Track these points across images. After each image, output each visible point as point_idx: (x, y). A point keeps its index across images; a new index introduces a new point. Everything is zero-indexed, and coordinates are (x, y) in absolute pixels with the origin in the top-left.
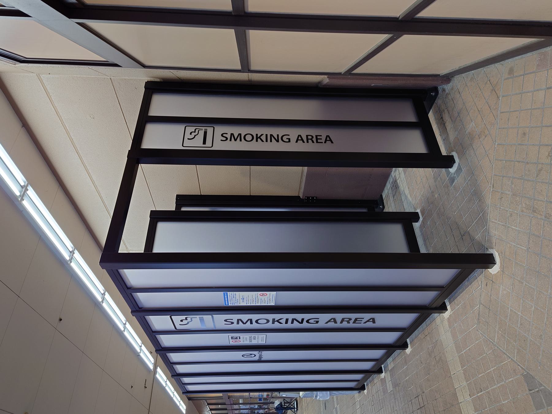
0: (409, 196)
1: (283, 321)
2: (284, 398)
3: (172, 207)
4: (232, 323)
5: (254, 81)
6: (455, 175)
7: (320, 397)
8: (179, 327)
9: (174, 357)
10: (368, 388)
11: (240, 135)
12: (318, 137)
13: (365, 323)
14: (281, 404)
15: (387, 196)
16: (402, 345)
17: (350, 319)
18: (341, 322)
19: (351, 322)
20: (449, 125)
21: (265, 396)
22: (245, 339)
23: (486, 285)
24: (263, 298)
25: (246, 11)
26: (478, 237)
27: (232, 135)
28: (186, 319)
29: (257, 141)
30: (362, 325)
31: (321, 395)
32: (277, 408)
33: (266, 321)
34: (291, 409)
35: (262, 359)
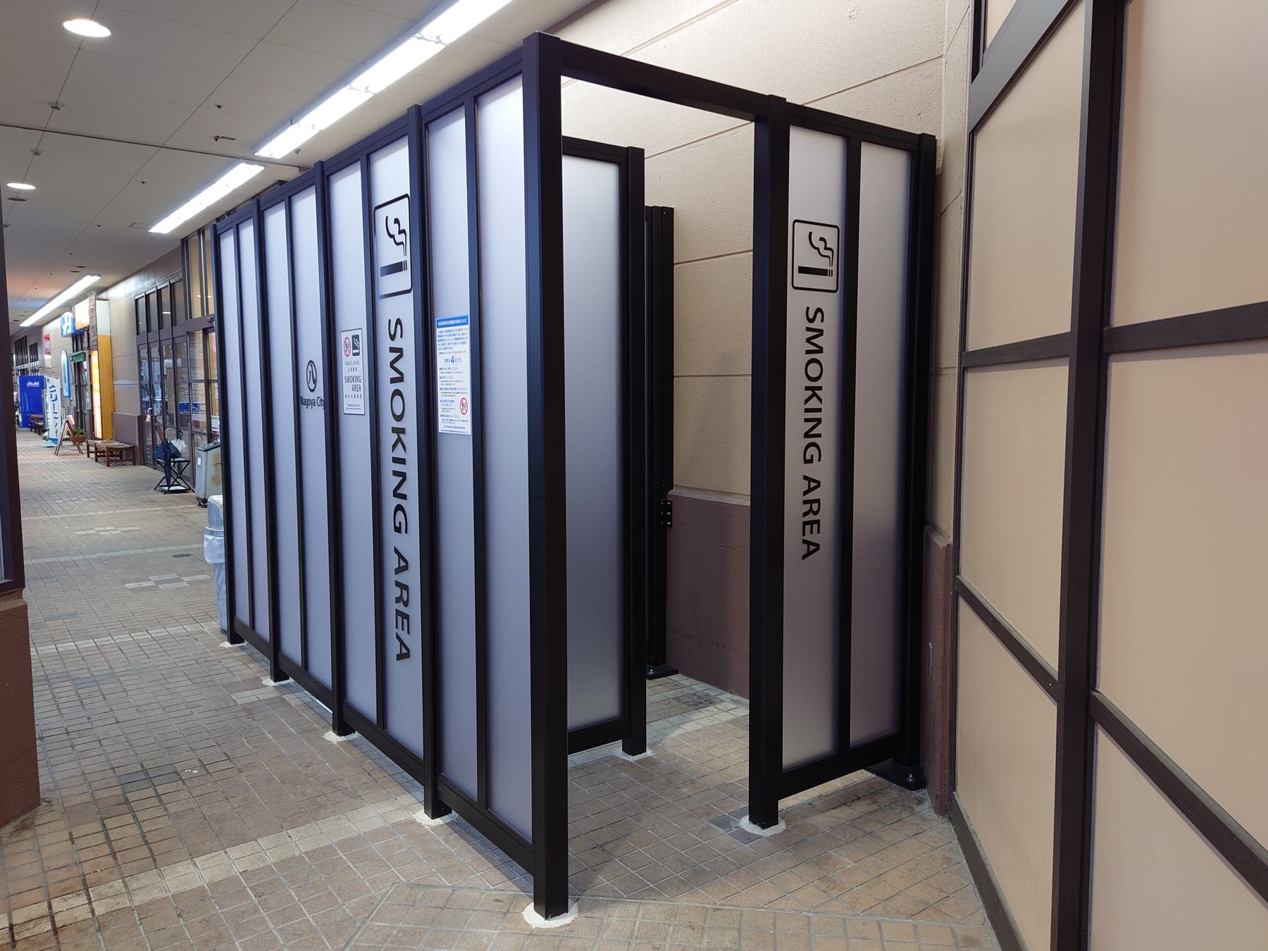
0: (680, 731)
1: (399, 453)
2: (192, 462)
3: (651, 200)
4: (393, 337)
5: (937, 382)
6: (734, 830)
7: (210, 542)
8: (381, 215)
9: (306, 206)
10: (235, 650)
11: (820, 350)
12: (815, 526)
13: (398, 637)
14: (177, 454)
15: (676, 685)
16: (345, 721)
17: (406, 604)
18: (397, 584)
19: (401, 607)
20: (844, 814)
21: (195, 417)
22: (353, 367)
23: (497, 900)
24: (457, 405)
25: (1112, 357)
26: (602, 880)
27: (820, 333)
28: (402, 232)
29: (807, 388)
30: (392, 630)
31: (216, 543)
32: (167, 446)
33: (398, 413)
34: (168, 478)
35: (303, 408)
